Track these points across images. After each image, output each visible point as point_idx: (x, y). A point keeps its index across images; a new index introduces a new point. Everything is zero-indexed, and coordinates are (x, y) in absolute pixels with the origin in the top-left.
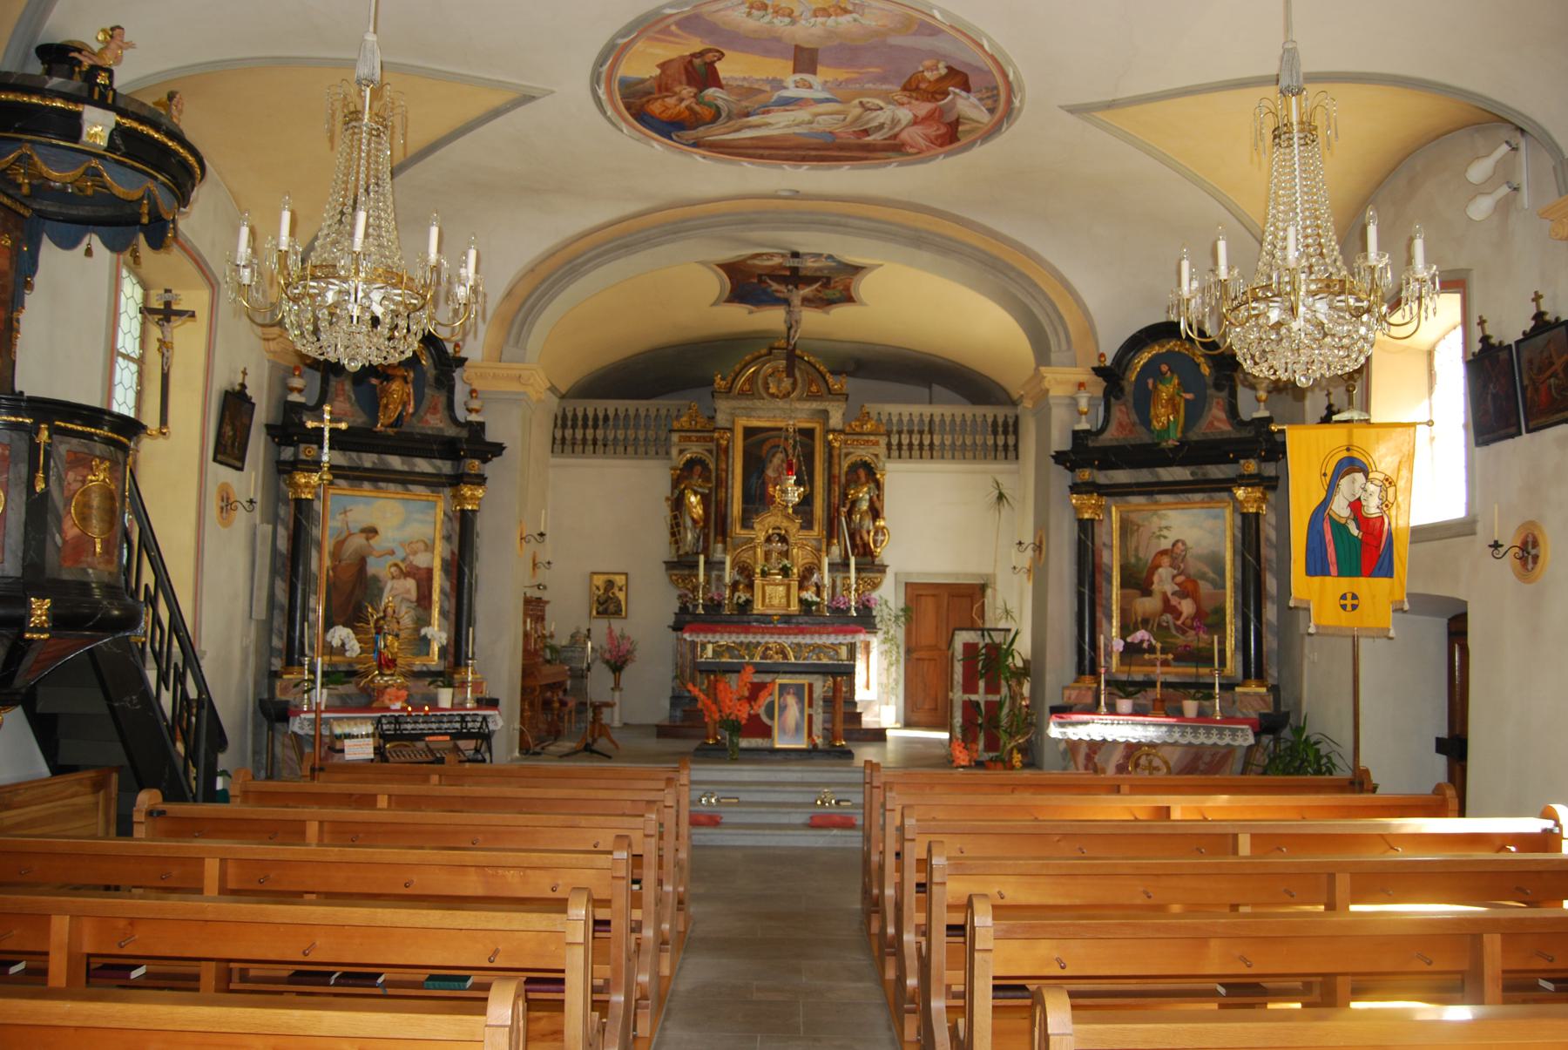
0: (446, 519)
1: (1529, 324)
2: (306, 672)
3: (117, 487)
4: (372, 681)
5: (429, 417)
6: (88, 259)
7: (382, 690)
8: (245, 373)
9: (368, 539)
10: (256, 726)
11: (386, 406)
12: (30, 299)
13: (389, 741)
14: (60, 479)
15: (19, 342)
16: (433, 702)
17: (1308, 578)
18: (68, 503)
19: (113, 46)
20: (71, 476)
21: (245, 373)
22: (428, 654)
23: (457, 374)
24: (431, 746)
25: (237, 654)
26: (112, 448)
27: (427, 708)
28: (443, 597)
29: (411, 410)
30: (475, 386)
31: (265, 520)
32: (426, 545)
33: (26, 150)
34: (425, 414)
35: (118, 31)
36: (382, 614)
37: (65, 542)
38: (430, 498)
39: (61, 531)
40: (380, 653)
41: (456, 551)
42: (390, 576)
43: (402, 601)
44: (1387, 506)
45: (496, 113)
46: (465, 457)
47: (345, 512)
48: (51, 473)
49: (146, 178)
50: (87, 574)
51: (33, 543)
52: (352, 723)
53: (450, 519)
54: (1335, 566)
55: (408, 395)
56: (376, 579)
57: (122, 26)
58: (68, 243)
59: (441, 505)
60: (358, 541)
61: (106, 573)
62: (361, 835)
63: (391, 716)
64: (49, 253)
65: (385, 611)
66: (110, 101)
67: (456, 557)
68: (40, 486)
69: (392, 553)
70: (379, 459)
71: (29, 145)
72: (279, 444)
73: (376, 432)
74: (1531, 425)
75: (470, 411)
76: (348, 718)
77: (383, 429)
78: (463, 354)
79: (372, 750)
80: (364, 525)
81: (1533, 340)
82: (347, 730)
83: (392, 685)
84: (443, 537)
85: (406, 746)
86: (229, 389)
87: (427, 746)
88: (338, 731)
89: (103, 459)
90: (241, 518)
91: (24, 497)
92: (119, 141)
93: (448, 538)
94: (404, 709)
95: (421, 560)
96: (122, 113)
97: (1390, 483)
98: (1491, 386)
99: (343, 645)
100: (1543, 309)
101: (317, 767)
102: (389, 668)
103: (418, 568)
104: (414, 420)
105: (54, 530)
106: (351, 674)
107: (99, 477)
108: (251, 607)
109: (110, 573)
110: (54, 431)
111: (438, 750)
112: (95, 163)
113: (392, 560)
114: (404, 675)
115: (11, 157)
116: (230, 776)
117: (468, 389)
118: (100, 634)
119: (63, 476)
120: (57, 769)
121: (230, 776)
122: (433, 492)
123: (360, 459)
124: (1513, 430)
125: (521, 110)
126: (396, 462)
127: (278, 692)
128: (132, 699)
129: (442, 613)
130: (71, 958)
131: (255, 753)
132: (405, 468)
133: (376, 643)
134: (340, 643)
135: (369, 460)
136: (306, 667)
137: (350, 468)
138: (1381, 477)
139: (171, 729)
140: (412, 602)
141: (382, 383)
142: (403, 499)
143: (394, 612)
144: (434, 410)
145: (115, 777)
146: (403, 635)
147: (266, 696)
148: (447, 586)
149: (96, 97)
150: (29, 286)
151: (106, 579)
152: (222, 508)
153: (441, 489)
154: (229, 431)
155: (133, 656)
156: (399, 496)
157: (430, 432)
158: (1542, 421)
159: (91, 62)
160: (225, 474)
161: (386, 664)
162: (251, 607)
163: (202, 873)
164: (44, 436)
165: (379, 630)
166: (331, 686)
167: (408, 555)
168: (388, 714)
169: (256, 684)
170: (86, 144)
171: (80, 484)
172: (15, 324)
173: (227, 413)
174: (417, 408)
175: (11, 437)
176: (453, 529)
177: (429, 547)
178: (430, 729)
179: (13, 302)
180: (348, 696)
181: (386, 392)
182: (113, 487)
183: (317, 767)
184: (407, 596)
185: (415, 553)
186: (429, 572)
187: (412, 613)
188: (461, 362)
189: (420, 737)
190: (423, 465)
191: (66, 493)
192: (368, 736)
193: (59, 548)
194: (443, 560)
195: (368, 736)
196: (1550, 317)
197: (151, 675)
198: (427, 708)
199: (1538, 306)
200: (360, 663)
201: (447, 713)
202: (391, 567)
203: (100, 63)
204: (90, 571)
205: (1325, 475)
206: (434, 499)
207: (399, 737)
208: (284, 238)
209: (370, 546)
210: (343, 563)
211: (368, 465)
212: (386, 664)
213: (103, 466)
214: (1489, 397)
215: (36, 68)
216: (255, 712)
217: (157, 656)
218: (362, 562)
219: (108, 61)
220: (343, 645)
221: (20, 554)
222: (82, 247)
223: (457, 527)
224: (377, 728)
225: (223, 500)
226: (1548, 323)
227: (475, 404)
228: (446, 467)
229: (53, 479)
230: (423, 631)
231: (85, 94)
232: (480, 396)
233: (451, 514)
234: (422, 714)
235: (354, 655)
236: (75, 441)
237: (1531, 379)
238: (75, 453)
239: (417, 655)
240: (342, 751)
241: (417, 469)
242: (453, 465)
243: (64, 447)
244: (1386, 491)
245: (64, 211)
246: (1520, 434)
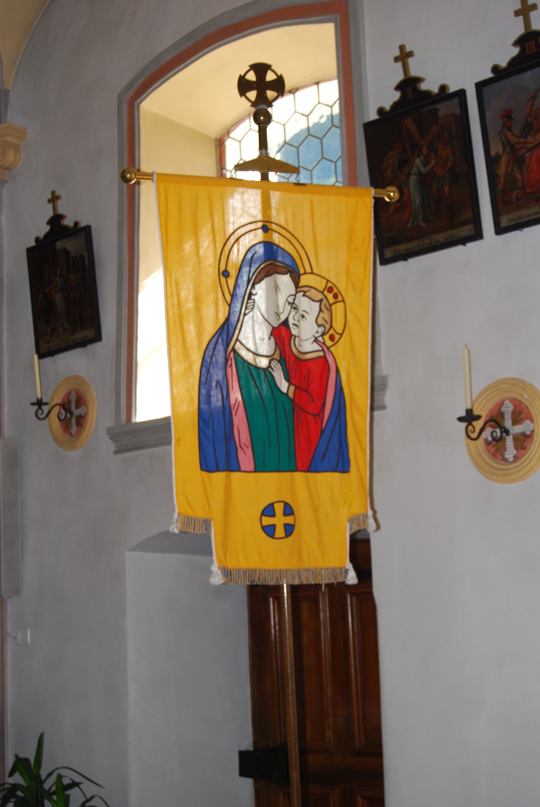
1: (44, 229)
17: (205, 474)
44: (332, 338)
54: (249, 451)
74: (504, 222)
81: (516, 80)
97: (335, 296)
98: (418, 162)
100: (61, 211)
124: (467, 230)
138: (320, 284)
158: (414, 245)
196: (68, 222)
199: (527, 22)
205: (226, 274)
214: (413, 179)
226: (66, 228)
237: (506, 144)
244: (330, 311)
246: (478, 235)
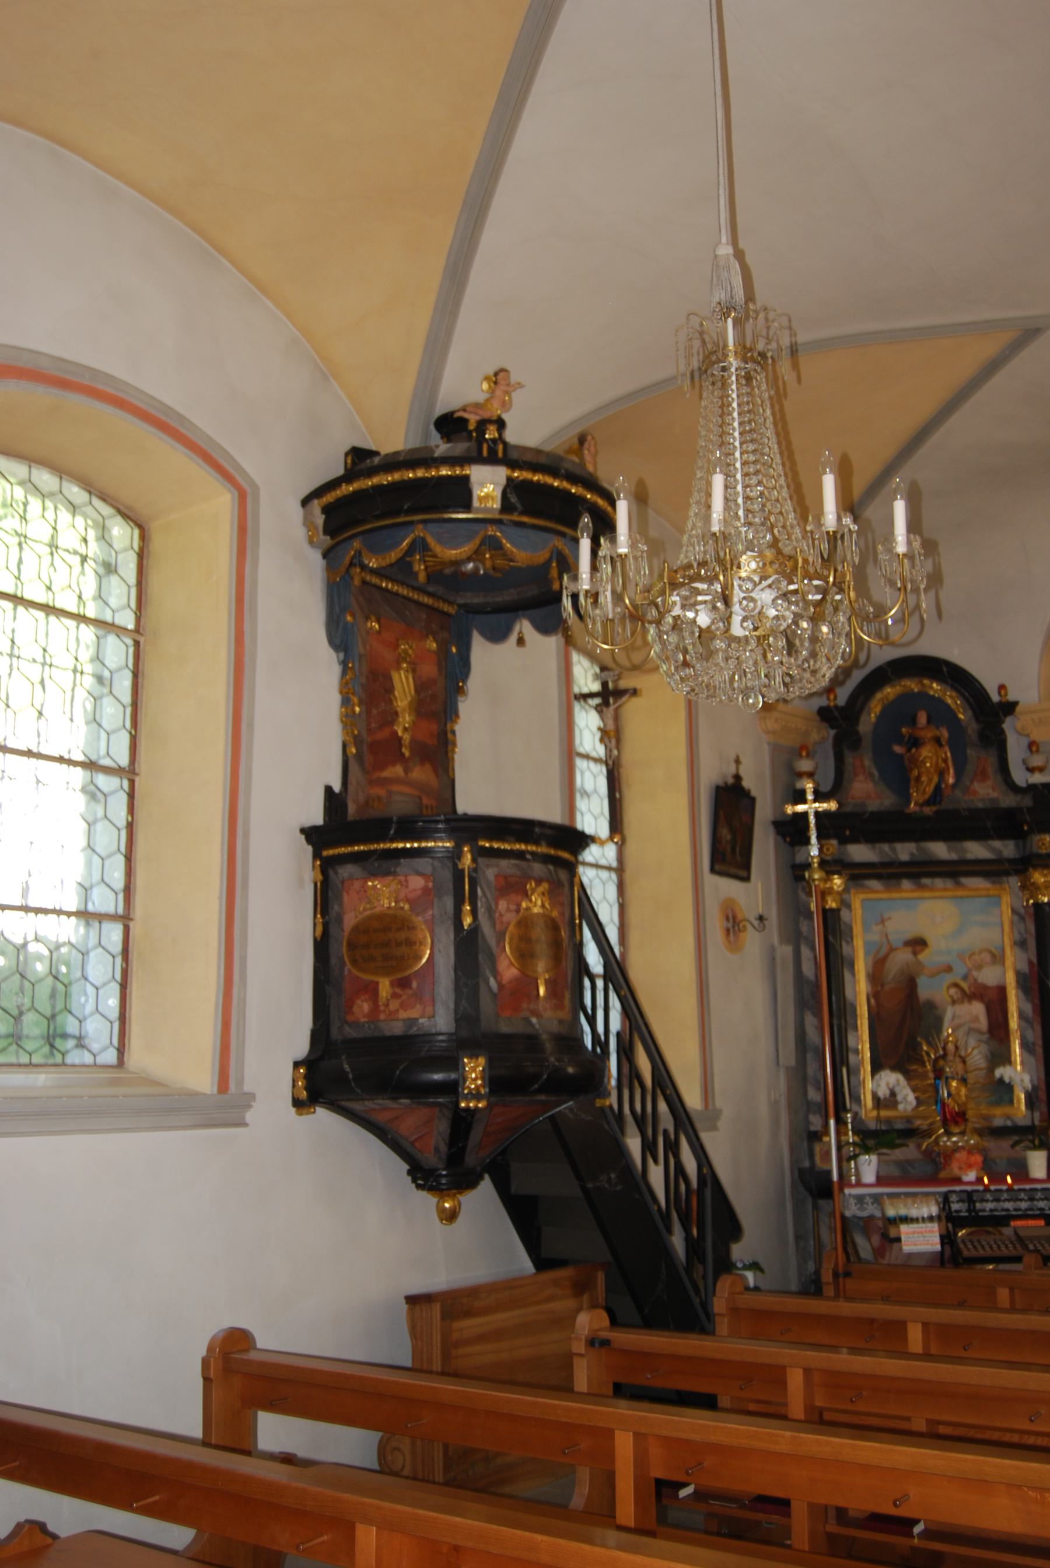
0: (1016, 918)
2: (850, 1133)
3: (562, 914)
4: (936, 1142)
5: (977, 786)
6: (521, 650)
7: (949, 1155)
8: (738, 761)
9: (915, 953)
10: (798, 1205)
11: (918, 779)
12: (465, 707)
13: (962, 1227)
14: (490, 911)
15: (456, 757)
16: (1021, 1172)
18: (501, 937)
19: (498, 393)
20: (503, 905)
21: (738, 761)
22: (1011, 1102)
23: (1008, 725)
24: (1022, 1234)
25: (764, 1112)
26: (551, 867)
27: (1009, 1179)
28: (1024, 1024)
29: (951, 781)
30: (1035, 736)
31: (784, 939)
32: (994, 956)
33: (419, 531)
34: (972, 782)
35: (501, 375)
36: (941, 1052)
37: (501, 986)
38: (991, 892)
39: (496, 974)
40: (943, 1105)
41: (1035, 960)
42: (949, 1000)
43: (968, 1033)
45: (992, 368)
46: (1031, 831)
47: (883, 921)
48: (479, 904)
49: (551, 536)
50: (532, 1025)
51: (465, 990)
52: (909, 1201)
53: (1022, 918)
55: (945, 761)
56: (931, 1005)
57: (508, 369)
58: (497, 635)
59: (1006, 900)
60: (903, 956)
61: (555, 1022)
62: (865, 1393)
63: (962, 1191)
64: (481, 650)
65: (944, 1049)
66: (500, 454)
67: (1036, 969)
68: (467, 921)
69: (949, 969)
70: (918, 849)
71: (421, 526)
72: (792, 844)
73: (909, 814)
75: (1031, 770)
76: (907, 1195)
77: (917, 809)
78: (1011, 697)
79: (937, 1239)
80: (909, 935)
82: (903, 1212)
83: (963, 1148)
84: (1015, 943)
85: (988, 1233)
86: (721, 783)
87: (1016, 1233)
88: (891, 1212)
89: (539, 882)
90: (752, 940)
91: (452, 936)
92: (513, 499)
93: (1021, 944)
94: (980, 1180)
95: (989, 976)
96: (512, 465)
99: (893, 1094)
101: (841, 1270)
102: (956, 1123)
103: (985, 987)
104: (958, 793)
105: (488, 973)
106: (910, 1133)
107: (537, 903)
108: (777, 1051)
109: (561, 1022)
110: (480, 853)
111: (1031, 1239)
112: (492, 531)
113: (948, 979)
114: (980, 1132)
115: (404, 544)
116: (762, 1270)
117: (1025, 742)
118: (553, 1098)
119: (493, 906)
120: (542, 1263)
121: (762, 1270)
122: (993, 883)
123: (894, 850)
125: (1026, 354)
126: (940, 850)
127: (817, 1159)
128: (610, 1178)
129: (1024, 1045)
130: (640, 1479)
131: (798, 1238)
132: (954, 856)
133: (937, 1091)
134: (888, 1093)
135: (904, 851)
136: (850, 1126)
137: (883, 865)
139: (666, 1218)
140: (981, 1033)
141: (909, 750)
142: (956, 897)
143: (957, 1048)
144: (983, 776)
145: (601, 1276)
146: (971, 1078)
147: (806, 1164)
148: (1028, 1008)
149: (485, 453)
150: (460, 691)
151: (555, 1027)
152: (728, 931)
153: (1005, 879)
154: (725, 834)
155: (608, 1123)
156: (950, 893)
157: (981, 805)
159: (478, 418)
160: (727, 887)
161: (954, 1119)
162: (777, 1051)
163: (614, 1444)
164: (467, 860)
165: (939, 1074)
166: (885, 1151)
167: (970, 970)
168: (958, 1188)
169: (793, 1148)
170: (478, 510)
171: (514, 914)
172: (449, 735)
173: (721, 813)
174: (958, 775)
175: (432, 865)
176: (1026, 931)
177: (998, 958)
178: (1003, 1210)
179: (445, 712)
180: (910, 1163)
181: (915, 762)
182: (555, 914)
183: (841, 1270)
184: (973, 1025)
185: (979, 967)
186: (1001, 991)
187: (984, 1048)
188: (1010, 708)
189: (1001, 1220)
190: (976, 850)
191: (498, 927)
192: (931, 1219)
193: (494, 995)
194: (1018, 973)
195: (931, 1219)
197: (634, 1144)
198: (1009, 1179)
200: (918, 1117)
201: (1039, 1186)
202: (948, 988)
203: (486, 415)
204: (534, 1020)
206: (997, 893)
207: (975, 1220)
208: (622, 538)
209: (919, 963)
210: (887, 988)
211: (904, 857)
212: (954, 1119)
213: (541, 889)
215: (435, 438)
216: (793, 1186)
217: (640, 1122)
218: (910, 984)
219: (494, 410)
220: (893, 1094)
221: (452, 1006)
222: (513, 638)
223: (1031, 927)
224: (944, 1209)
225: (727, 919)
227: (1037, 761)
228: (1008, 849)
229: (481, 911)
230: (998, 1072)
231: (475, 454)
232: (1041, 749)
233: (1022, 911)
234: (1004, 1187)
235: (909, 1108)
236: (504, 863)
238: (506, 878)
239: (998, 1103)
240: (898, 1240)
241: (970, 856)
242: (1017, 846)
243: (491, 872)
245: (489, 599)
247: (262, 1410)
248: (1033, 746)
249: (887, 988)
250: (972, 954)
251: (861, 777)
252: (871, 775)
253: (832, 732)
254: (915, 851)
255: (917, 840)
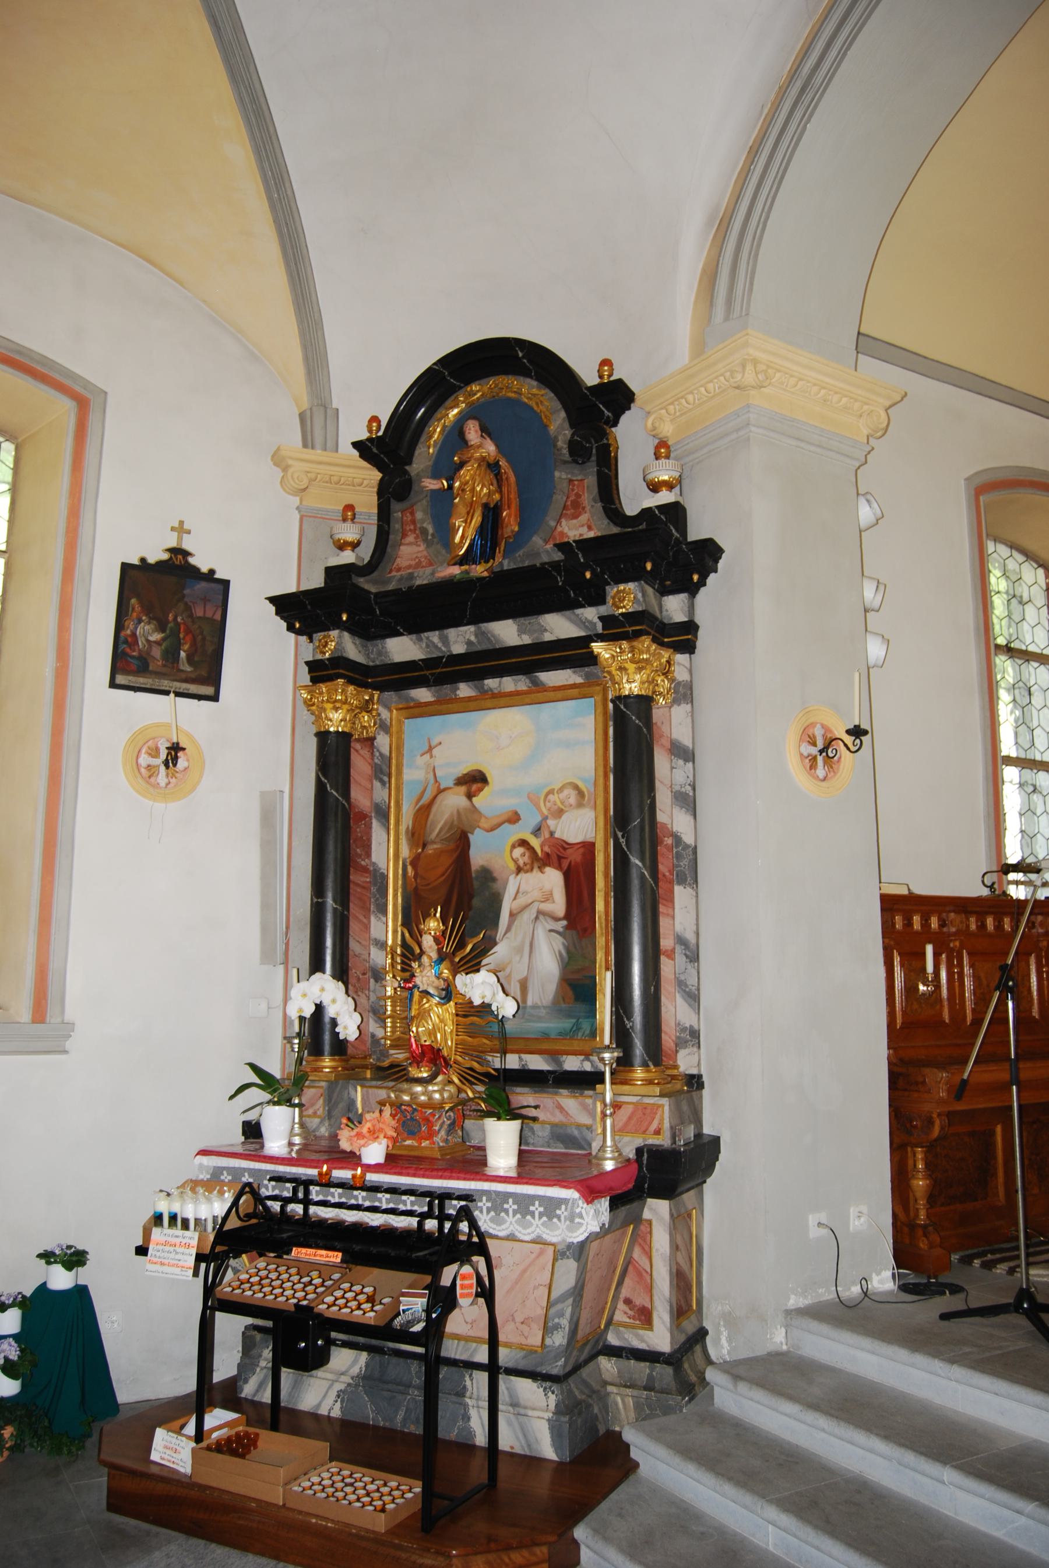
9: (470, 796)
34: (559, 522)
42: (512, 866)
56: (487, 875)
60: (455, 801)
69: (514, 818)
80: (464, 769)
103: (564, 845)
123: (445, 640)
132: (527, 640)
185: (559, 813)
202: (513, 847)
209: (474, 809)
211: (459, 649)
218: (461, 842)
247: (445, 1328)
248: (662, 449)
249: (430, 850)
250: (551, 792)
251: (411, 538)
252: (424, 531)
253: (377, 475)
254: (473, 638)
255: (475, 620)
